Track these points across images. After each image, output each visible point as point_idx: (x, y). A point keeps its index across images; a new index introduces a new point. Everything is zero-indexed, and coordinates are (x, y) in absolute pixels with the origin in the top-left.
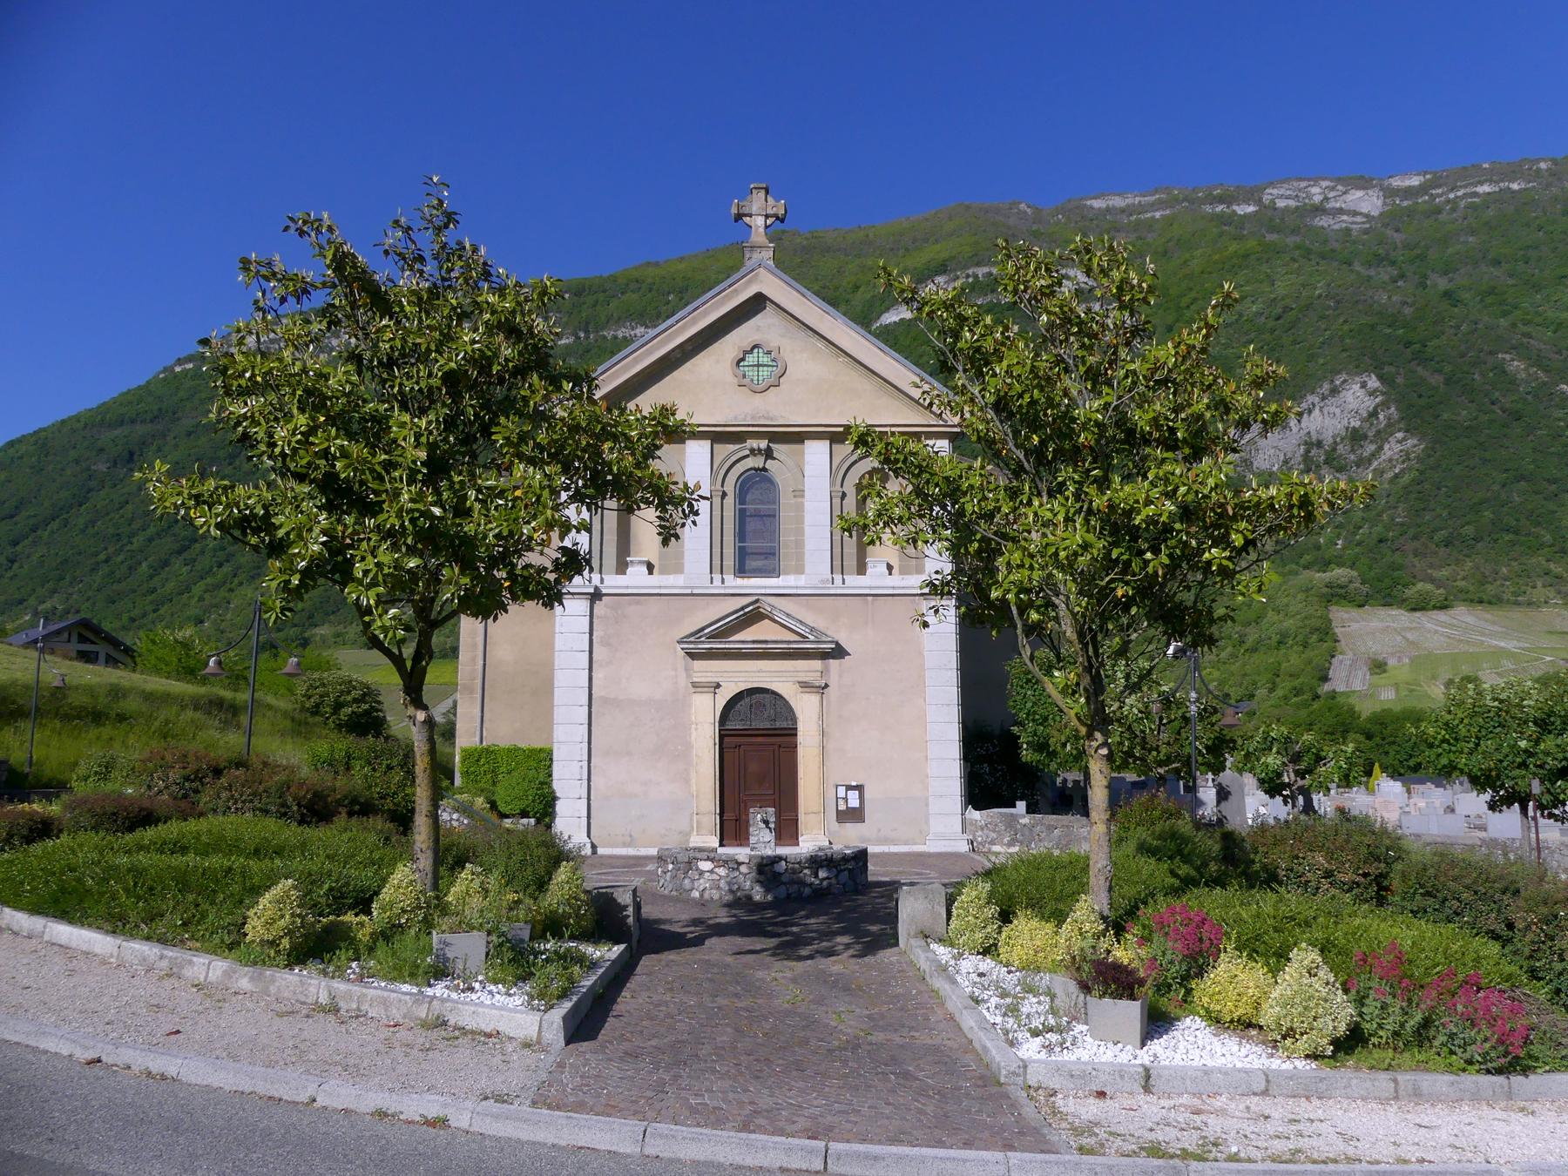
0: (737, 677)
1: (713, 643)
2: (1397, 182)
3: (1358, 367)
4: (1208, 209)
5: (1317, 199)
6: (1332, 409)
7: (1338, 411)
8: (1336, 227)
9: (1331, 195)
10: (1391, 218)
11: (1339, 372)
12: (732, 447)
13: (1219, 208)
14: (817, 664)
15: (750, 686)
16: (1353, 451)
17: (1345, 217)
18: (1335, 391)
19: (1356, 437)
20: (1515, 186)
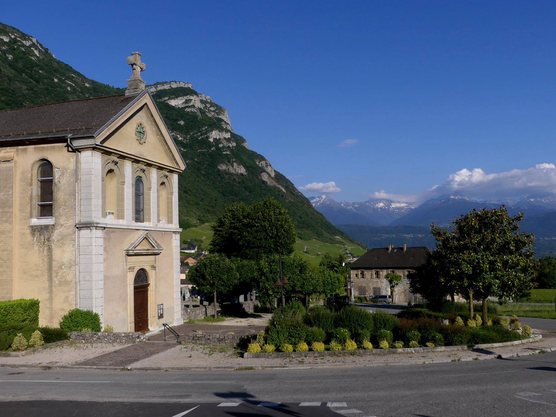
14: (152, 257)
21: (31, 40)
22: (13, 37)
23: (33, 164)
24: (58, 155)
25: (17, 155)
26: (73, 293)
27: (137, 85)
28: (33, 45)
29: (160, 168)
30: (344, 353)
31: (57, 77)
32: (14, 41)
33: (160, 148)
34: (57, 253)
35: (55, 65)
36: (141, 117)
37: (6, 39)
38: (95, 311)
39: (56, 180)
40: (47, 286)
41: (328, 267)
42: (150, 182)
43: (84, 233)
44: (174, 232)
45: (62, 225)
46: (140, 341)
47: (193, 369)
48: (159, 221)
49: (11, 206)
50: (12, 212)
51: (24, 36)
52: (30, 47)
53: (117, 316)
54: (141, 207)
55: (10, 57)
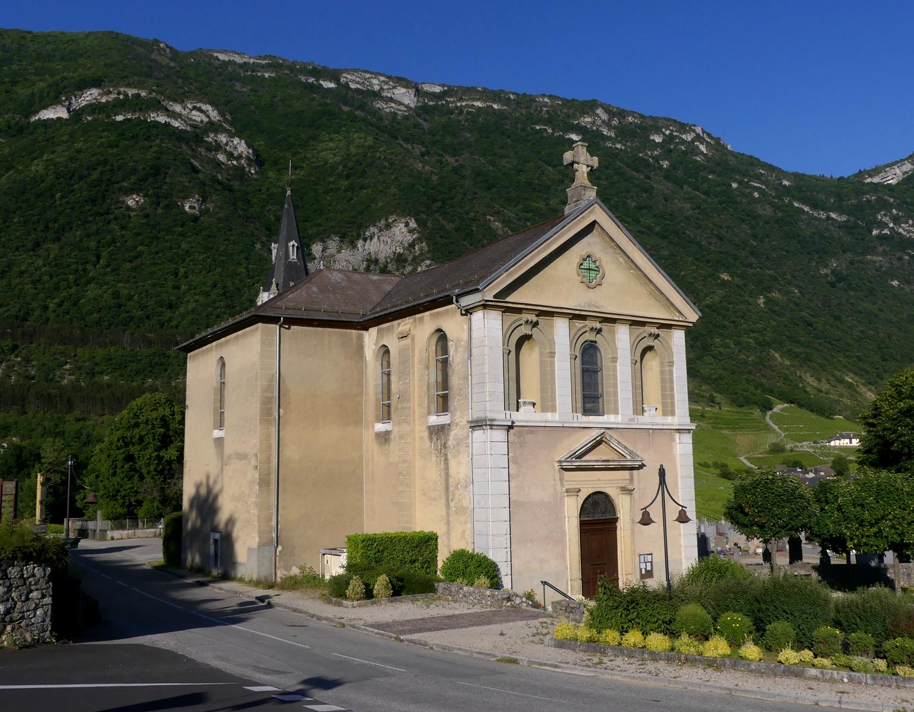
0: (590, 483)
1: (576, 463)
2: (427, 88)
3: (405, 211)
4: (303, 79)
5: (377, 88)
6: (386, 239)
7: (389, 240)
8: (388, 110)
9: (386, 87)
10: (422, 111)
11: (392, 214)
12: (517, 316)
13: (311, 80)
14: (626, 474)
15: (595, 490)
16: (398, 269)
17: (393, 105)
18: (388, 226)
19: (400, 260)
20: (495, 106)
21: (694, 131)
22: (668, 132)
23: (430, 338)
24: (450, 320)
25: (415, 327)
26: (469, 525)
27: (580, 194)
28: (698, 138)
29: (636, 323)
30: (736, 662)
31: (735, 180)
32: (670, 139)
33: (640, 289)
34: (452, 463)
35: (732, 161)
37: (658, 139)
38: (491, 556)
39: (451, 359)
40: (444, 514)
42: (615, 349)
43: (478, 434)
44: (679, 431)
45: (457, 425)
46: (513, 606)
47: (455, 651)
48: (639, 409)
51: (684, 127)
52: (693, 141)
53: (558, 565)
54: (600, 391)
55: (665, 164)
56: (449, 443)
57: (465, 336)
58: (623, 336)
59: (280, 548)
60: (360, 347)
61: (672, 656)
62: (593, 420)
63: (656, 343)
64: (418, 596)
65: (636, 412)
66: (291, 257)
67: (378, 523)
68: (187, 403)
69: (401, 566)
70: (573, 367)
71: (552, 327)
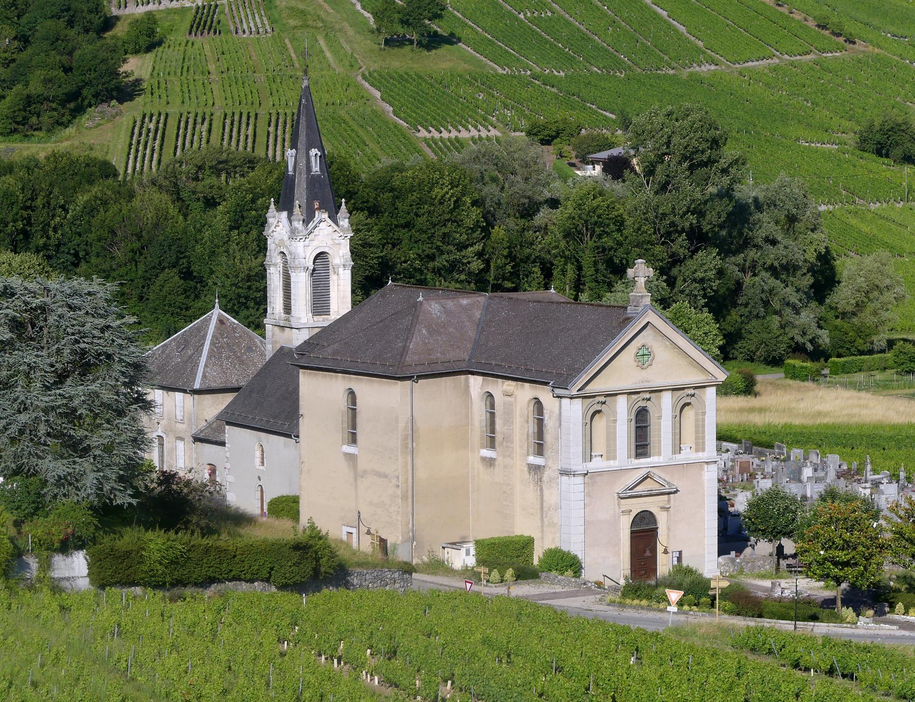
0: (637, 506)
26: (558, 535)
34: (546, 493)
36: (646, 338)
41: (60, 606)
43: (565, 478)
48: (677, 448)
49: (512, 442)
50: (513, 448)
53: (610, 562)
56: (544, 479)
57: (557, 410)
58: (667, 399)
59: (415, 543)
60: (467, 386)
61: (649, 608)
62: (643, 461)
63: (692, 400)
64: (530, 581)
65: (674, 453)
66: (314, 169)
67: (492, 529)
68: (301, 412)
69: (508, 557)
70: (629, 428)
71: (615, 402)
